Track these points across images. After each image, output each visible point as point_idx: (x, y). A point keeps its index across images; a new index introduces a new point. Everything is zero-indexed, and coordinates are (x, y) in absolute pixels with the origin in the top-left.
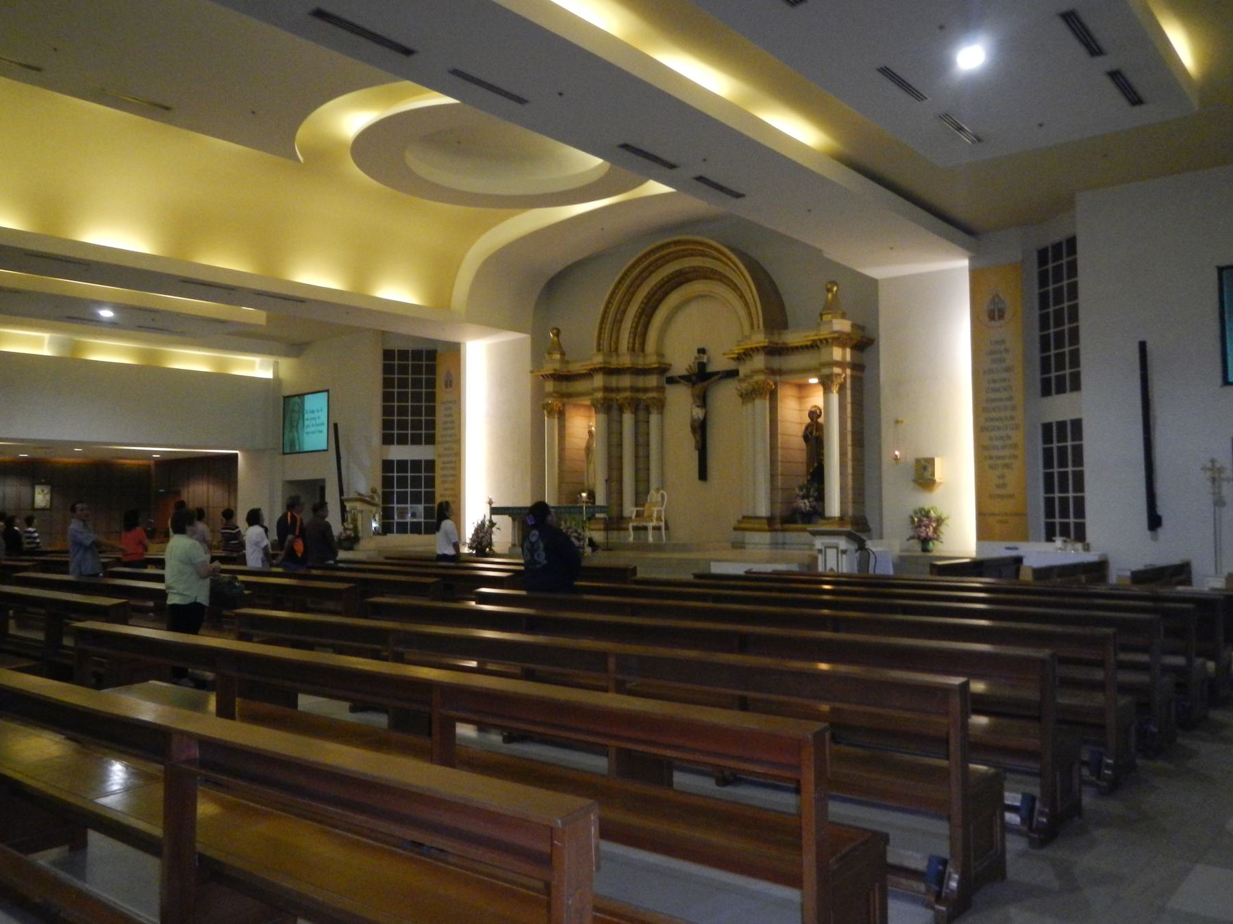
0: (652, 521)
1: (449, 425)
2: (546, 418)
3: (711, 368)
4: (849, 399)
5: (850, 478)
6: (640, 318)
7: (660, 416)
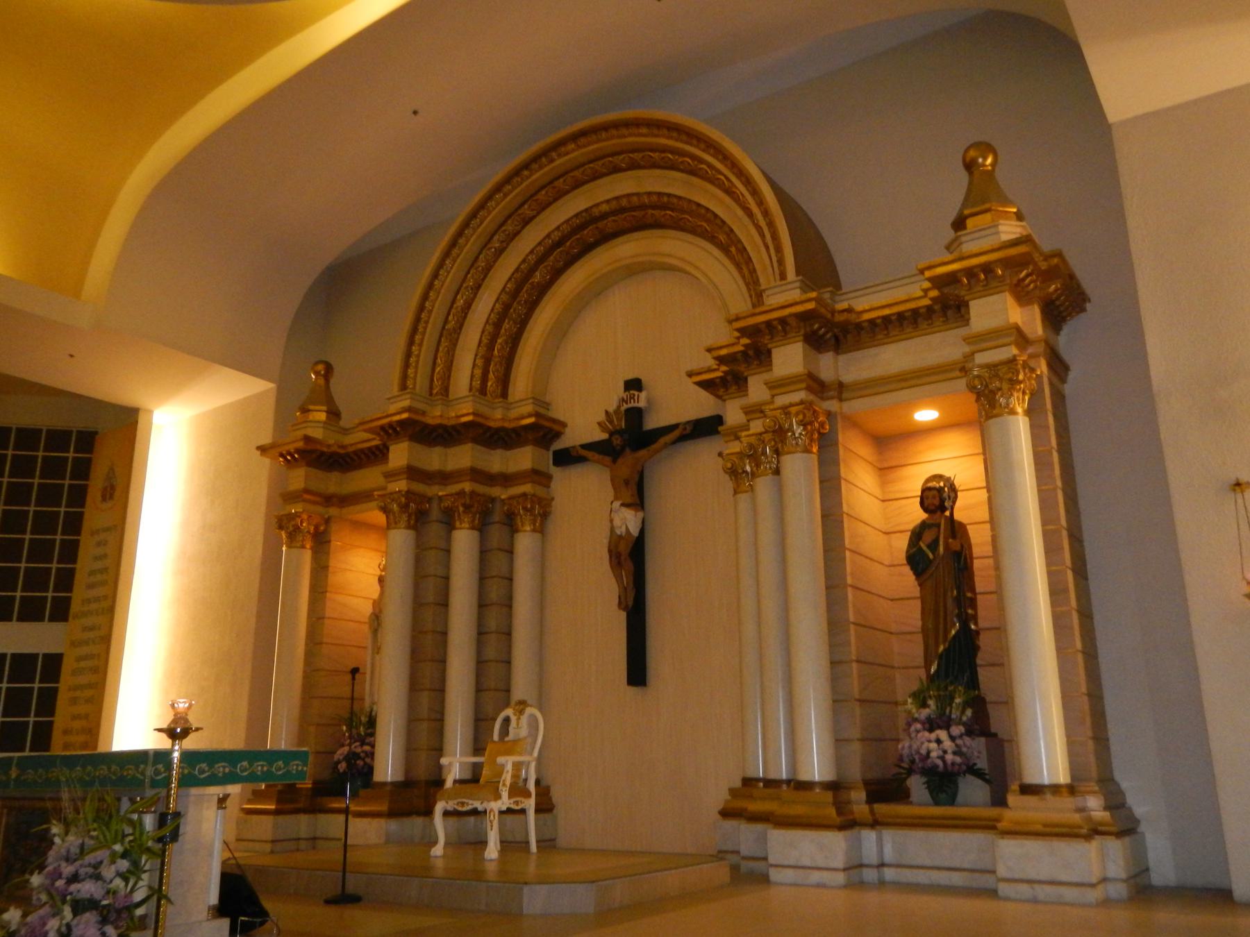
0: (498, 797)
1: (99, 577)
2: (284, 549)
3: (653, 422)
6: (498, 325)
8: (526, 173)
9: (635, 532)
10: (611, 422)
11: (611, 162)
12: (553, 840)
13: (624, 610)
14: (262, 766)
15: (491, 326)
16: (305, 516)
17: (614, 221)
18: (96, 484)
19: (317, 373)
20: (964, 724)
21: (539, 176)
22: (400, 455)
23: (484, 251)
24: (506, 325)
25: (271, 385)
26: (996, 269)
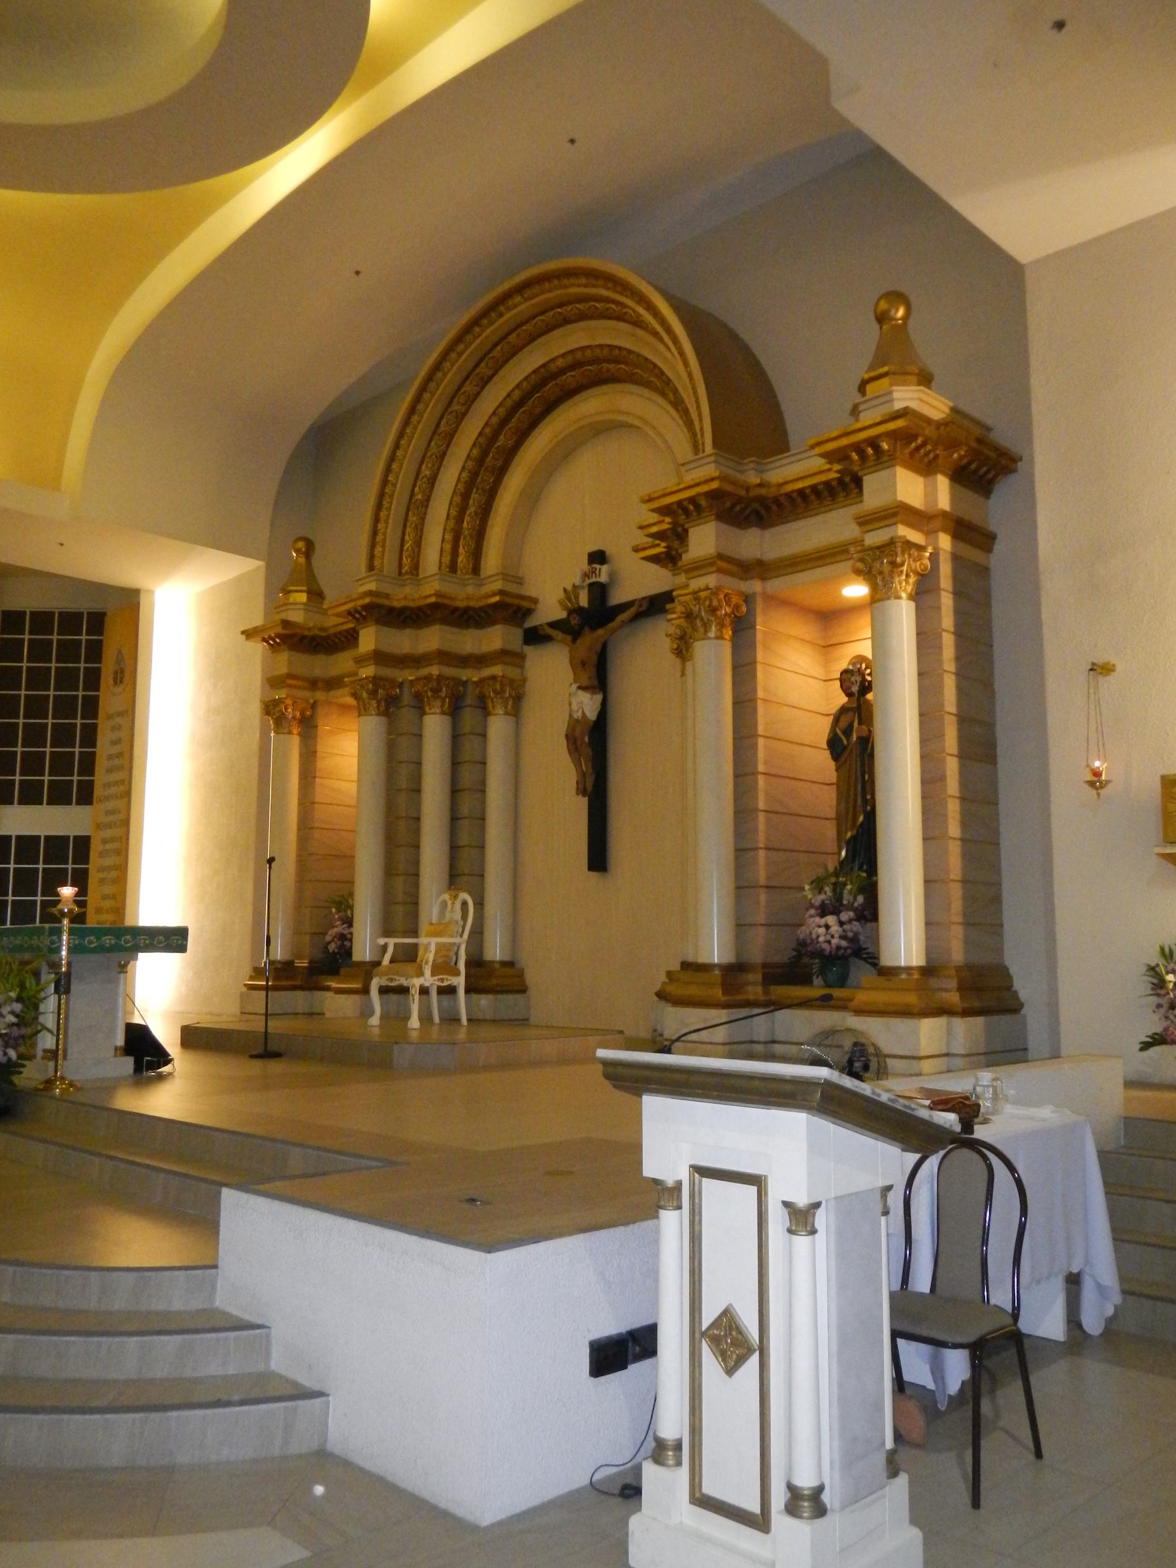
1: (116, 762)
3: (618, 597)
4: (947, 620)
5: (954, 851)
6: (466, 496)
7: (511, 719)
8: (477, 329)
9: (592, 715)
10: (569, 600)
11: (543, 320)
12: (527, 1020)
13: (584, 795)
14: (145, 940)
15: (459, 497)
16: (289, 702)
17: (572, 376)
18: (107, 668)
19: (297, 551)
20: (855, 910)
21: (489, 332)
22: (369, 639)
23: (445, 417)
24: (474, 496)
25: (261, 563)
26: (881, 444)
